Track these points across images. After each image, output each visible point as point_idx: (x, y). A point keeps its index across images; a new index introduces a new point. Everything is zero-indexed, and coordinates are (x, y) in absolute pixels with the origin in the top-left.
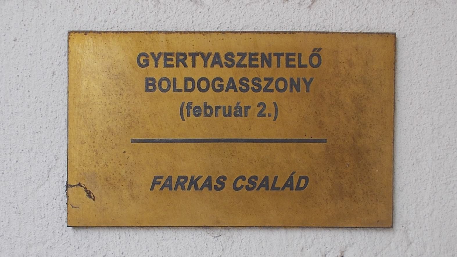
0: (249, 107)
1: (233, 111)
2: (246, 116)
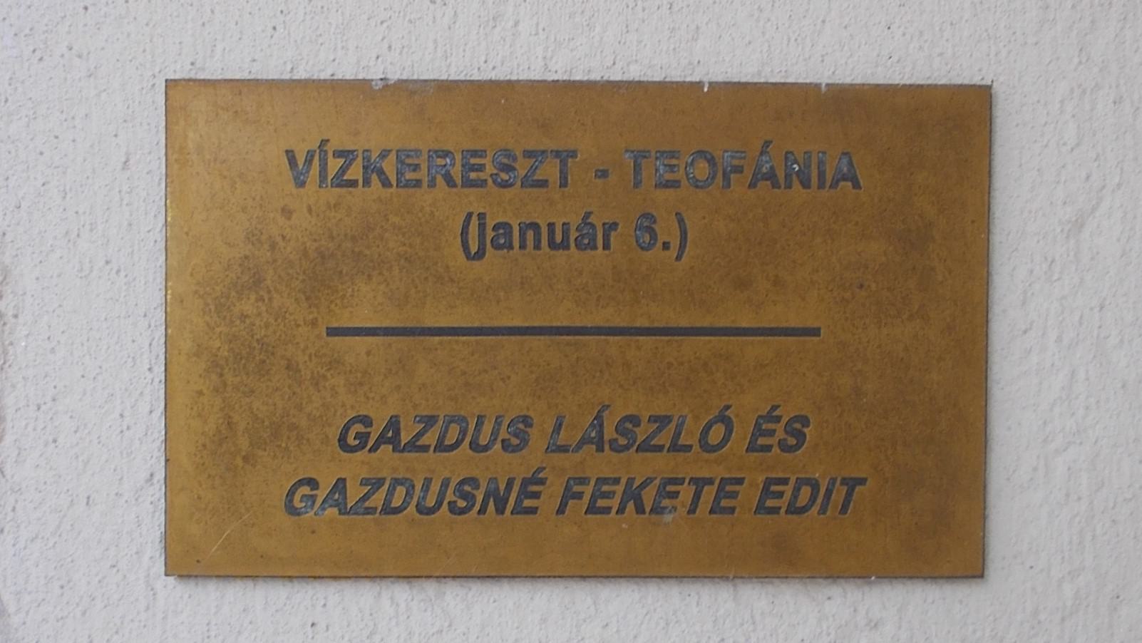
0: (614, 226)
1: (573, 235)
2: (606, 246)
